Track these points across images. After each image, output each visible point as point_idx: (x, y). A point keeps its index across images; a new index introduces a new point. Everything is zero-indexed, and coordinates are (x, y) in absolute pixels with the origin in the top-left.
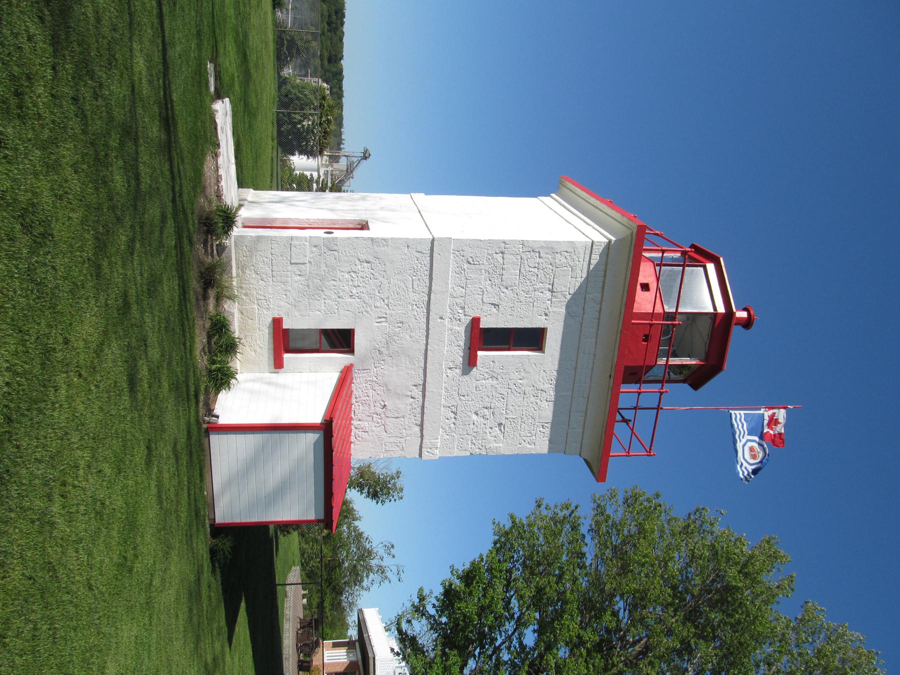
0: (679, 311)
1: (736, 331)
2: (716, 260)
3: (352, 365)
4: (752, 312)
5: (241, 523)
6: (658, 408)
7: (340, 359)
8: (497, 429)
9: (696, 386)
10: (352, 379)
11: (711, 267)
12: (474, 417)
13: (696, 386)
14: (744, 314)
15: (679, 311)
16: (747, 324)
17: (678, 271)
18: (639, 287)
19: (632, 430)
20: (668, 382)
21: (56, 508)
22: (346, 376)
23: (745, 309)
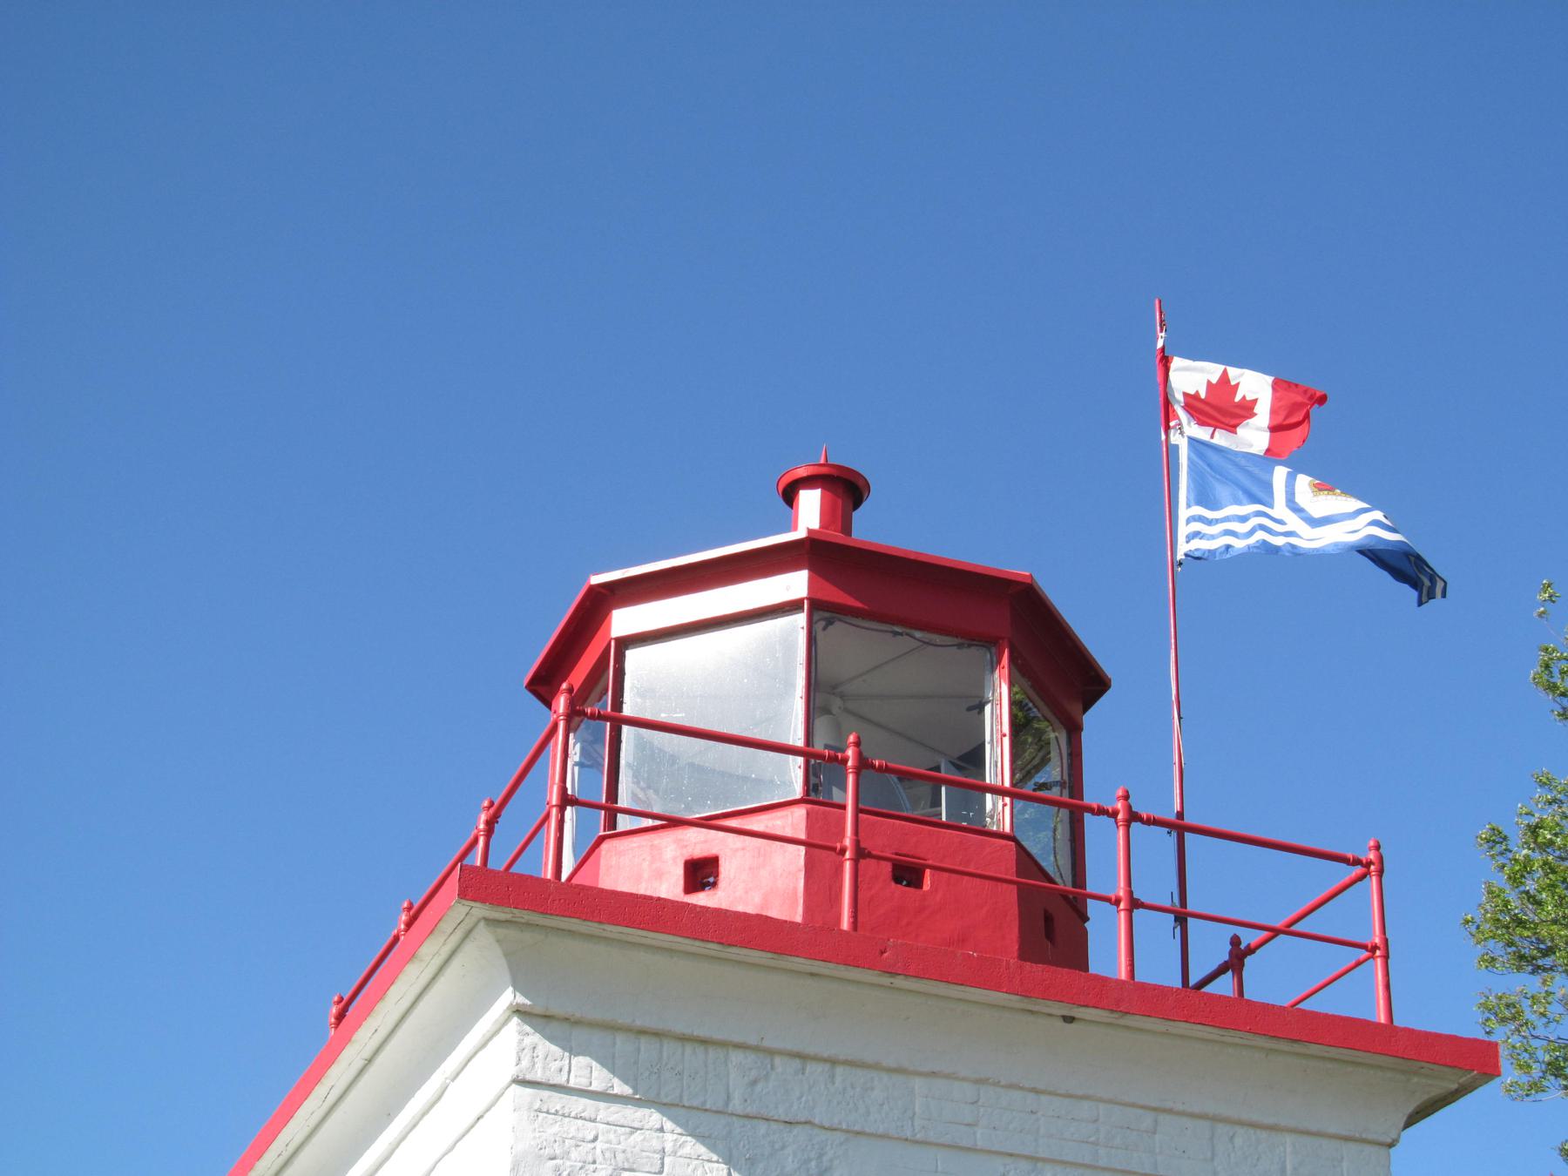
1: (872, 527)
4: (802, 472)
9: (1092, 684)
11: (624, 620)
13: (1092, 684)
16: (846, 489)
18: (701, 899)
23: (789, 495)
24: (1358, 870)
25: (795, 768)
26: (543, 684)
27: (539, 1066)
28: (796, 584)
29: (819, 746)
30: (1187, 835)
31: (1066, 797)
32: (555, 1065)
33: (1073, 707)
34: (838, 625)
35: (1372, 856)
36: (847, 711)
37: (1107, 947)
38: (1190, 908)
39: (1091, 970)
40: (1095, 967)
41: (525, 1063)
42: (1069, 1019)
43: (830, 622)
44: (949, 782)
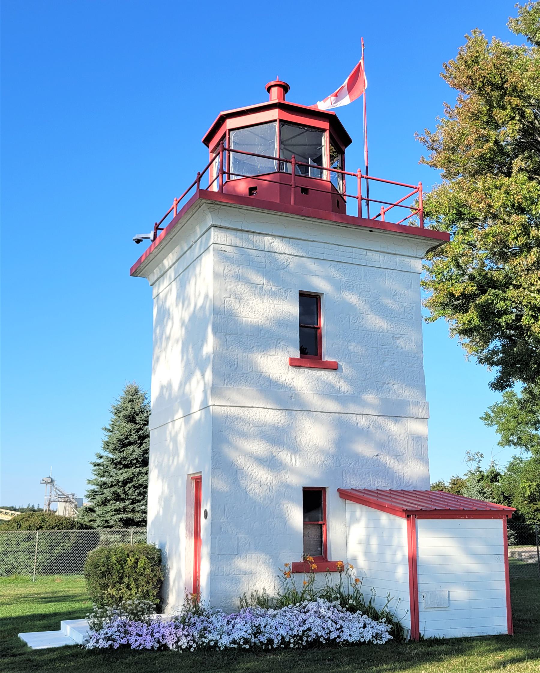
0: (277, 157)
1: (291, 100)
2: (223, 119)
3: (339, 490)
4: (273, 83)
5: (507, 607)
6: (367, 178)
7: (332, 500)
8: (398, 342)
9: (347, 141)
10: (352, 489)
11: (230, 123)
12: (387, 364)
13: (347, 141)
14: (275, 90)
15: (324, 171)
16: (285, 88)
17: (234, 154)
18: (251, 197)
19: (395, 205)
20: (343, 167)
21: (267, 635)
22: (346, 495)
23: (269, 90)
24: (416, 190)
25: (276, 162)
26: (207, 141)
27: (219, 239)
28: (274, 114)
29: (281, 158)
30: (231, 175)
31: (340, 171)
32: (223, 240)
33: (343, 148)
34: (285, 125)
35: (420, 186)
36: (285, 148)
37: (352, 210)
38: (370, 198)
39: (347, 214)
40: (349, 213)
41: (216, 239)
42: (371, 231)
43: (283, 125)
44: (311, 166)
